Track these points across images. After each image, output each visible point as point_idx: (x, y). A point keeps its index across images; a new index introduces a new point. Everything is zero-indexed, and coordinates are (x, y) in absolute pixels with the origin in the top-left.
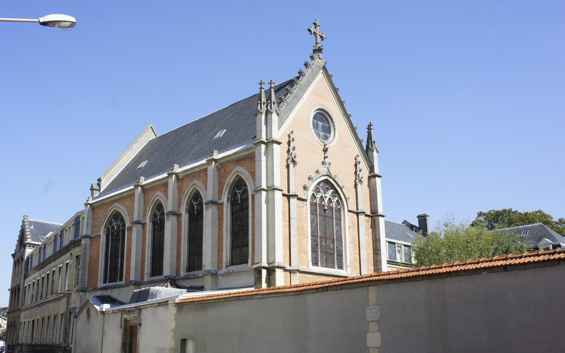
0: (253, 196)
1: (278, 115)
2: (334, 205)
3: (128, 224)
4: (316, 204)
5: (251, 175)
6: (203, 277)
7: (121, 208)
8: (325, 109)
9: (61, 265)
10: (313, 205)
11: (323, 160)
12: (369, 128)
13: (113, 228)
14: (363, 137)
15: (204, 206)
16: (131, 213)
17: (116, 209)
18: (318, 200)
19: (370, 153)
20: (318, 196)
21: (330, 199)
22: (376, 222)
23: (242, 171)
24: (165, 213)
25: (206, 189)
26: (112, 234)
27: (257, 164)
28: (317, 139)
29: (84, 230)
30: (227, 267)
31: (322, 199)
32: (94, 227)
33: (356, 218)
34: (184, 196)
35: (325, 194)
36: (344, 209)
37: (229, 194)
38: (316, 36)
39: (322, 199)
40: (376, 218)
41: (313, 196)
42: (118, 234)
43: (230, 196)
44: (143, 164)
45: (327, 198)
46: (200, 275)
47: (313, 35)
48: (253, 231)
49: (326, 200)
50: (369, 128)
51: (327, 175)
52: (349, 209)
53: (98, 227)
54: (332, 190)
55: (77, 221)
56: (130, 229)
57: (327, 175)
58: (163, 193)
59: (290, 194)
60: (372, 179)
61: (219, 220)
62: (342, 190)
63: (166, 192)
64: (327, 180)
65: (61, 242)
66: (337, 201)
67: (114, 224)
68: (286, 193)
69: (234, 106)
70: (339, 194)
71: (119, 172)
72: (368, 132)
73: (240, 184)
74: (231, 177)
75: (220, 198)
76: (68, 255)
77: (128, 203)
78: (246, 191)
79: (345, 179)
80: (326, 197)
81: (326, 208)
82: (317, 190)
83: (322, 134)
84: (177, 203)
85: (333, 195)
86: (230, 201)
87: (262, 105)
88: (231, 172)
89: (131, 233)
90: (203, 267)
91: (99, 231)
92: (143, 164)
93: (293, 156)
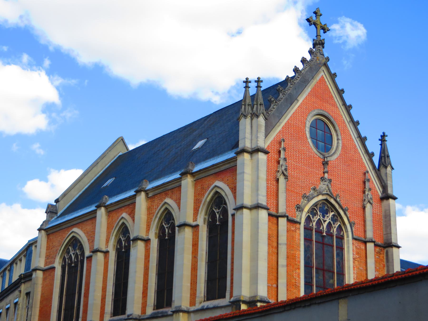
0: (233, 215)
1: (266, 119)
2: (334, 231)
3: (87, 253)
4: (311, 229)
5: (232, 191)
6: (172, 315)
7: (79, 232)
8: (326, 114)
9: (8, 306)
10: (308, 229)
11: (323, 175)
12: (383, 138)
13: (70, 258)
14: (374, 147)
15: (177, 228)
16: (91, 240)
17: (75, 235)
18: (314, 224)
19: (383, 170)
20: (316, 219)
21: (329, 223)
22: (390, 254)
23: (221, 185)
24: (131, 238)
25: (179, 209)
26: (70, 265)
27: (238, 177)
28: (315, 150)
29: (39, 261)
30: (201, 303)
31: (319, 223)
32: (50, 258)
33: (363, 248)
34: (154, 218)
35: (324, 217)
36: (348, 237)
37: (206, 215)
38: (316, 28)
39: (319, 223)
40: (390, 249)
41: (308, 219)
42: (76, 266)
43: (207, 217)
44: (109, 181)
45: (326, 223)
46: (170, 313)
47: (313, 26)
48: (232, 259)
49: (325, 225)
50: (383, 138)
51: (327, 194)
52: (355, 236)
53: (52, 258)
54: (333, 213)
55: (28, 250)
56: (90, 258)
57: (327, 194)
58: (130, 214)
59: (278, 214)
60: (385, 202)
61: (193, 246)
62: (345, 214)
63: (132, 214)
64: (326, 200)
65: (11, 278)
66: (340, 226)
67: (71, 253)
68: (274, 213)
69: (217, 113)
70: (341, 217)
71: (81, 192)
72: (381, 145)
73: (218, 200)
74: (209, 194)
75: (195, 219)
76: (17, 292)
77: (88, 227)
78: (225, 212)
79: (348, 199)
80: (325, 221)
81: (325, 234)
82: (313, 211)
83: (321, 144)
84: (145, 227)
85: (334, 219)
86: (206, 223)
87: (247, 106)
88: (209, 188)
89: (91, 263)
90: (173, 304)
91: (54, 262)
92: (109, 181)
93: (283, 168)
